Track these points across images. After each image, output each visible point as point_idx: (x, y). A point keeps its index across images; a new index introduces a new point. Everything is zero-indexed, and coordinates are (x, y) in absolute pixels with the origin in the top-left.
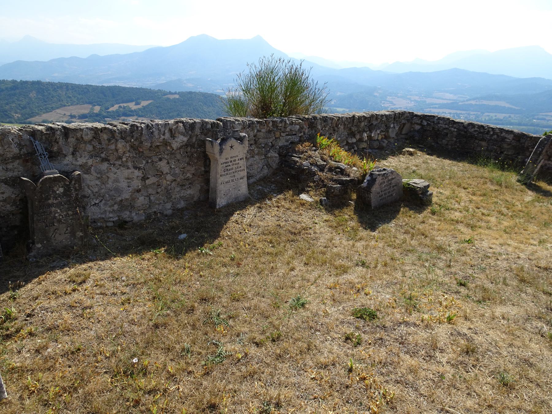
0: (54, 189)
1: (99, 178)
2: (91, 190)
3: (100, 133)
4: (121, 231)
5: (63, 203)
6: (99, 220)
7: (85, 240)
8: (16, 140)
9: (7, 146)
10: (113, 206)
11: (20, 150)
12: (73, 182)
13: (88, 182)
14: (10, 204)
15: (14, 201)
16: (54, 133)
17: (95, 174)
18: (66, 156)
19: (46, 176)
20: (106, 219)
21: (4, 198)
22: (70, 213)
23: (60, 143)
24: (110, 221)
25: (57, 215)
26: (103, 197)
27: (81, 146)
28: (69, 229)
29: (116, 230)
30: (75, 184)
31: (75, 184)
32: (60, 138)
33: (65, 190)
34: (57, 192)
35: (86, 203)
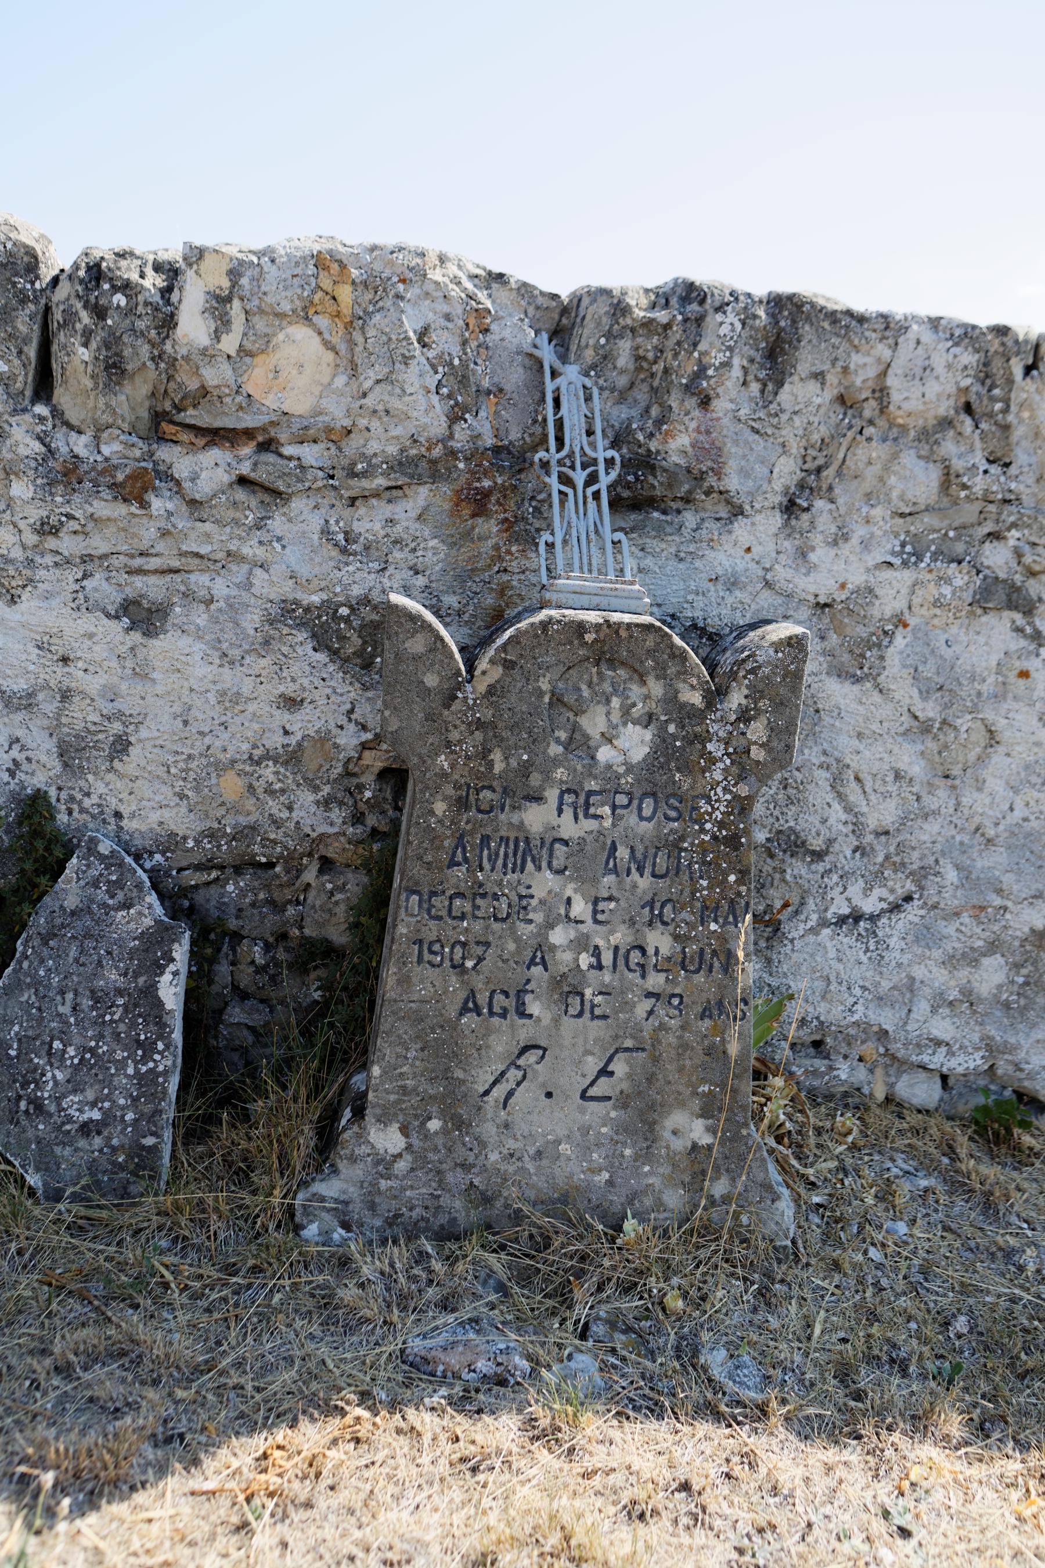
0: (584, 721)
1: (926, 728)
2: (848, 809)
3: (1018, 371)
4: (990, 1171)
5: (623, 853)
6: (849, 1041)
7: (720, 1188)
8: (445, 342)
9: (380, 370)
10: (972, 958)
11: (455, 417)
12: (736, 699)
13: (845, 744)
14: (316, 789)
15: (348, 774)
16: (700, 320)
17: (905, 692)
18: (738, 512)
19: (553, 613)
20: (898, 1048)
21: (293, 740)
22: (659, 941)
23: (721, 406)
24: (923, 1067)
25: (558, 936)
26: (921, 876)
27: (861, 453)
28: (619, 1067)
29: (950, 1151)
30: (745, 717)
31: (745, 717)
32: (727, 365)
33: (662, 748)
34: (605, 754)
35: (795, 900)
